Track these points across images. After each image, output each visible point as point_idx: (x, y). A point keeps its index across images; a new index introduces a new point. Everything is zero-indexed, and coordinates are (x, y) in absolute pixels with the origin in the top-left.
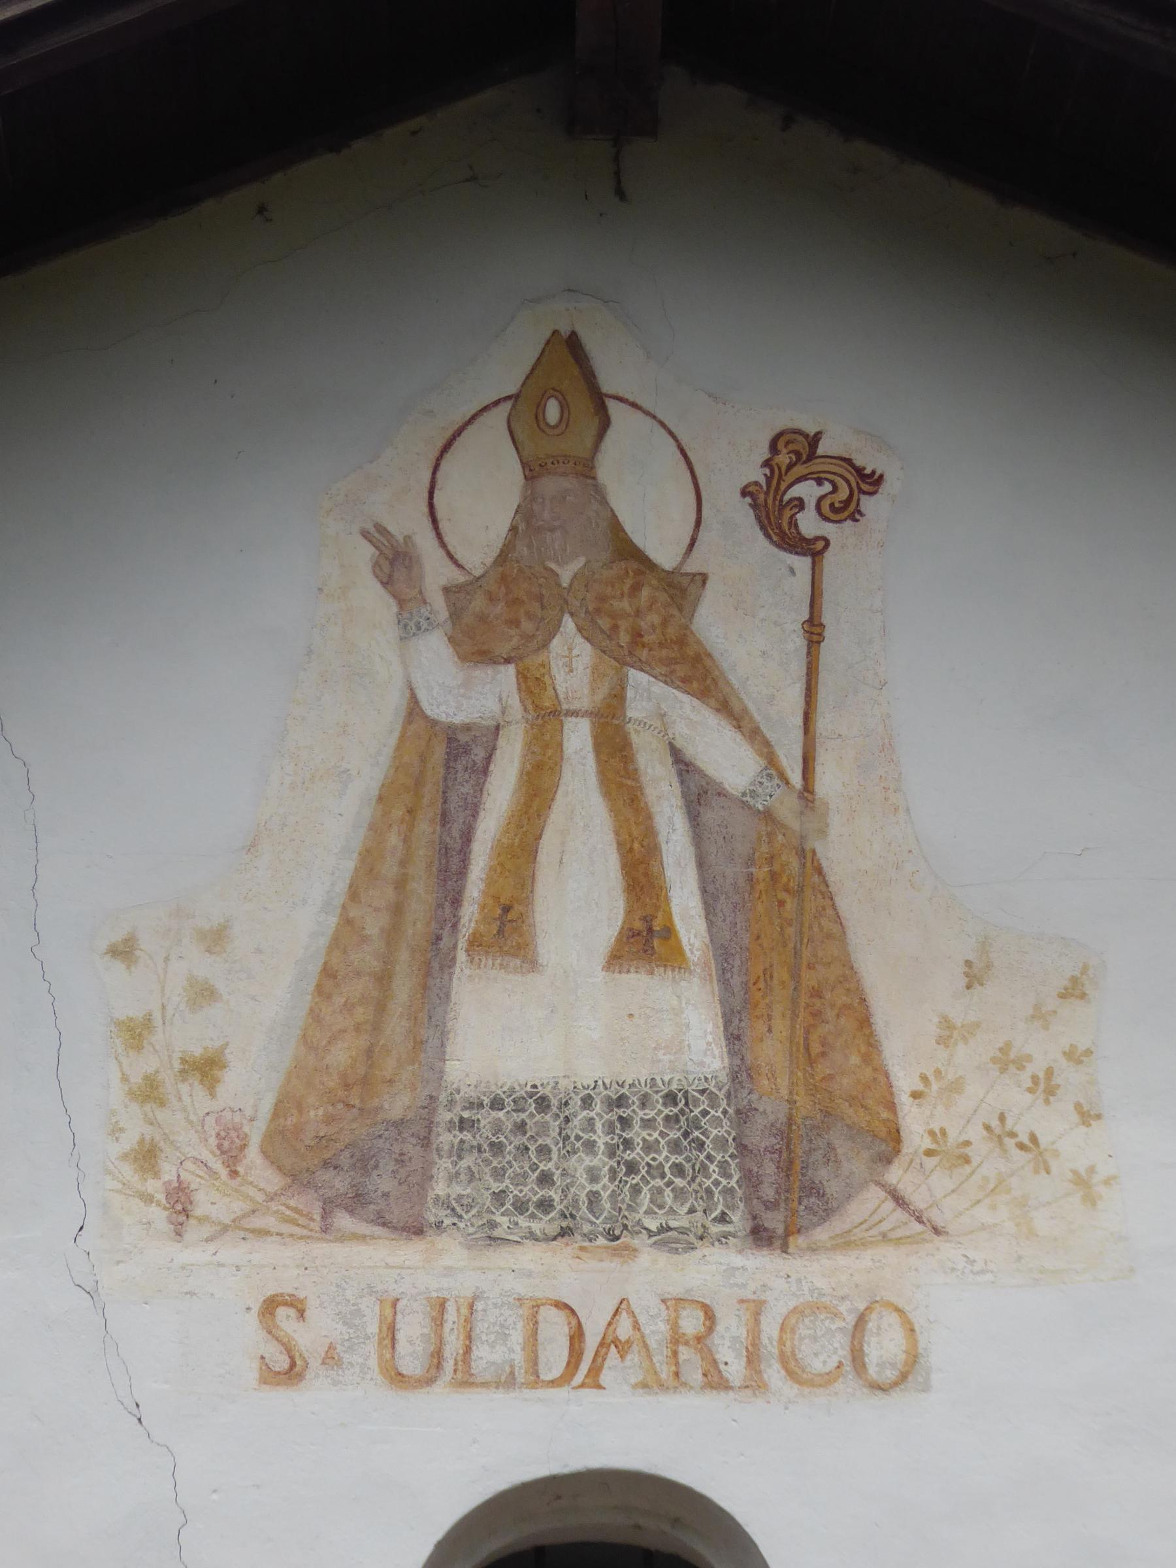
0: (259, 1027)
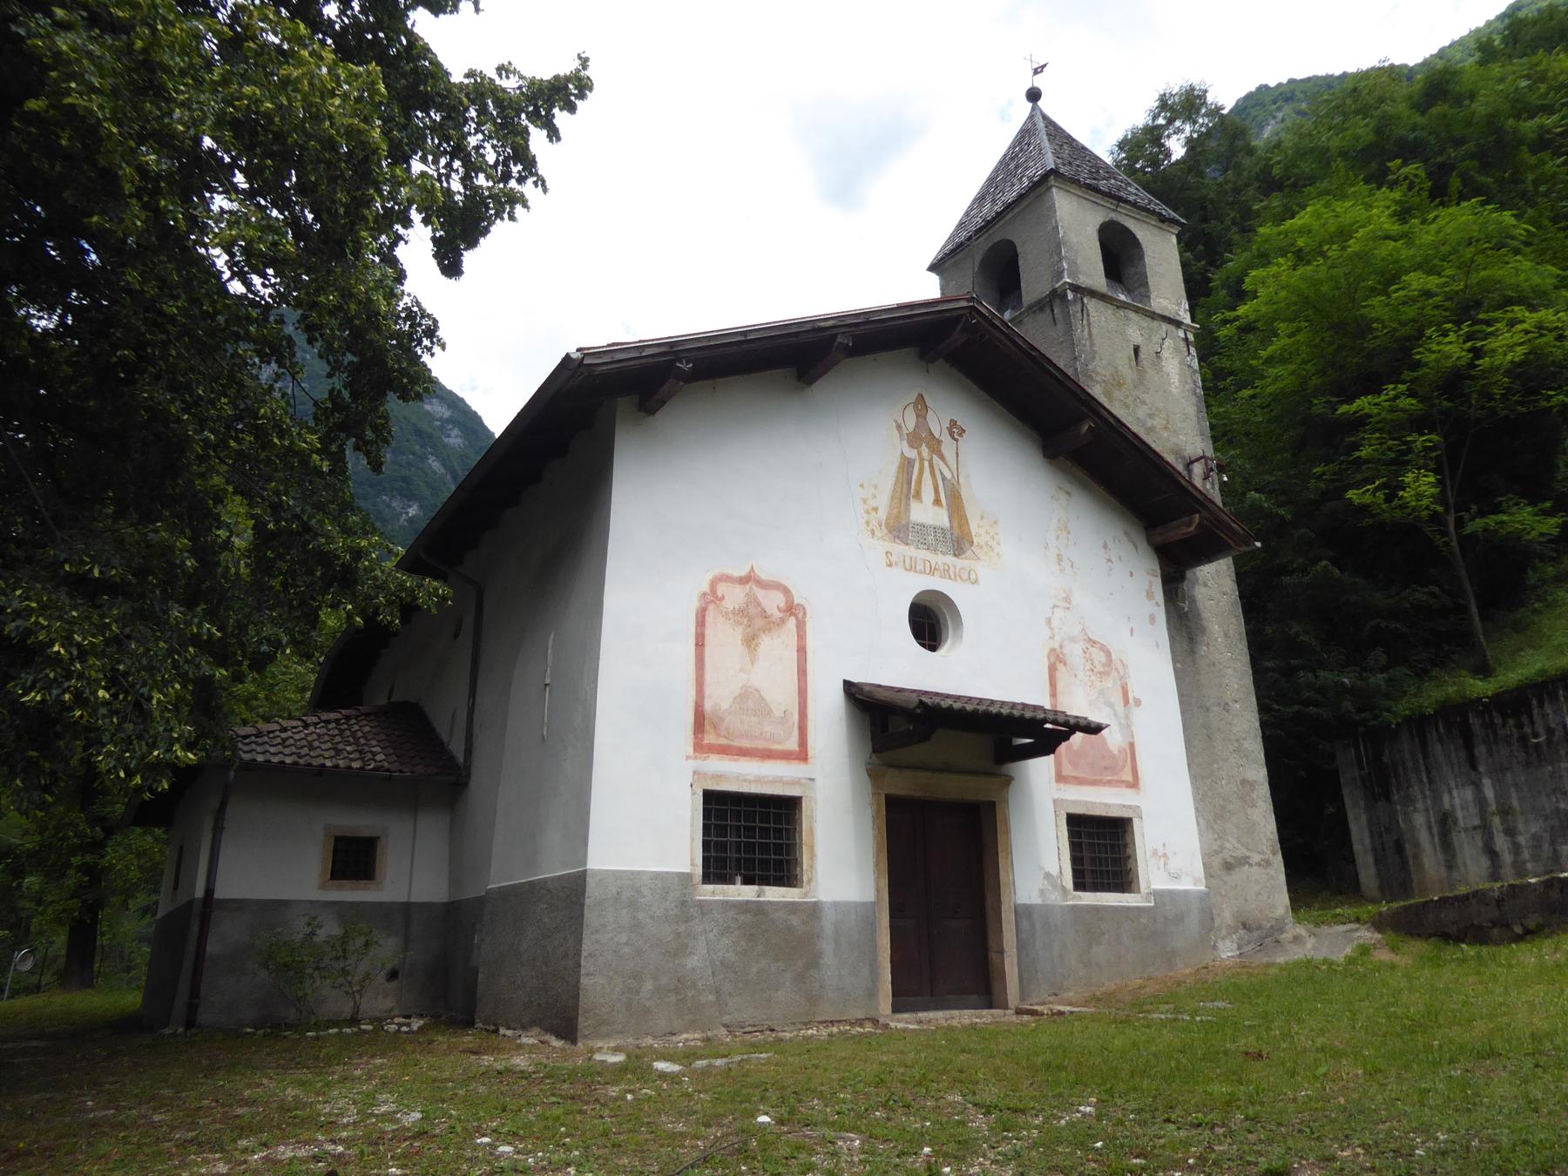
0: (883, 501)
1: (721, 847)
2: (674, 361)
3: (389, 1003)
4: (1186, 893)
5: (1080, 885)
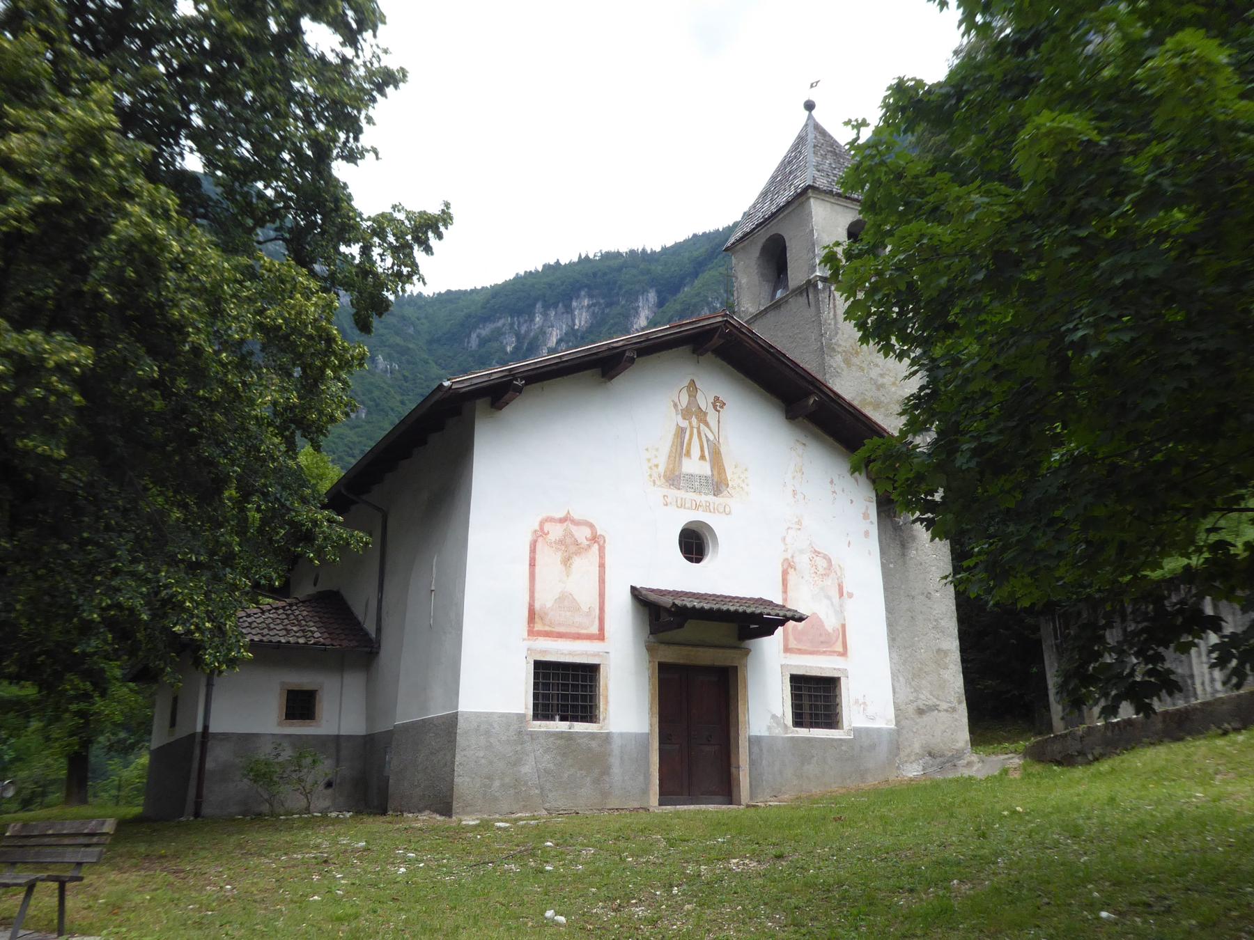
0: (662, 461)
1: (546, 697)
2: (511, 381)
3: (327, 803)
4: (879, 730)
5: (799, 721)
